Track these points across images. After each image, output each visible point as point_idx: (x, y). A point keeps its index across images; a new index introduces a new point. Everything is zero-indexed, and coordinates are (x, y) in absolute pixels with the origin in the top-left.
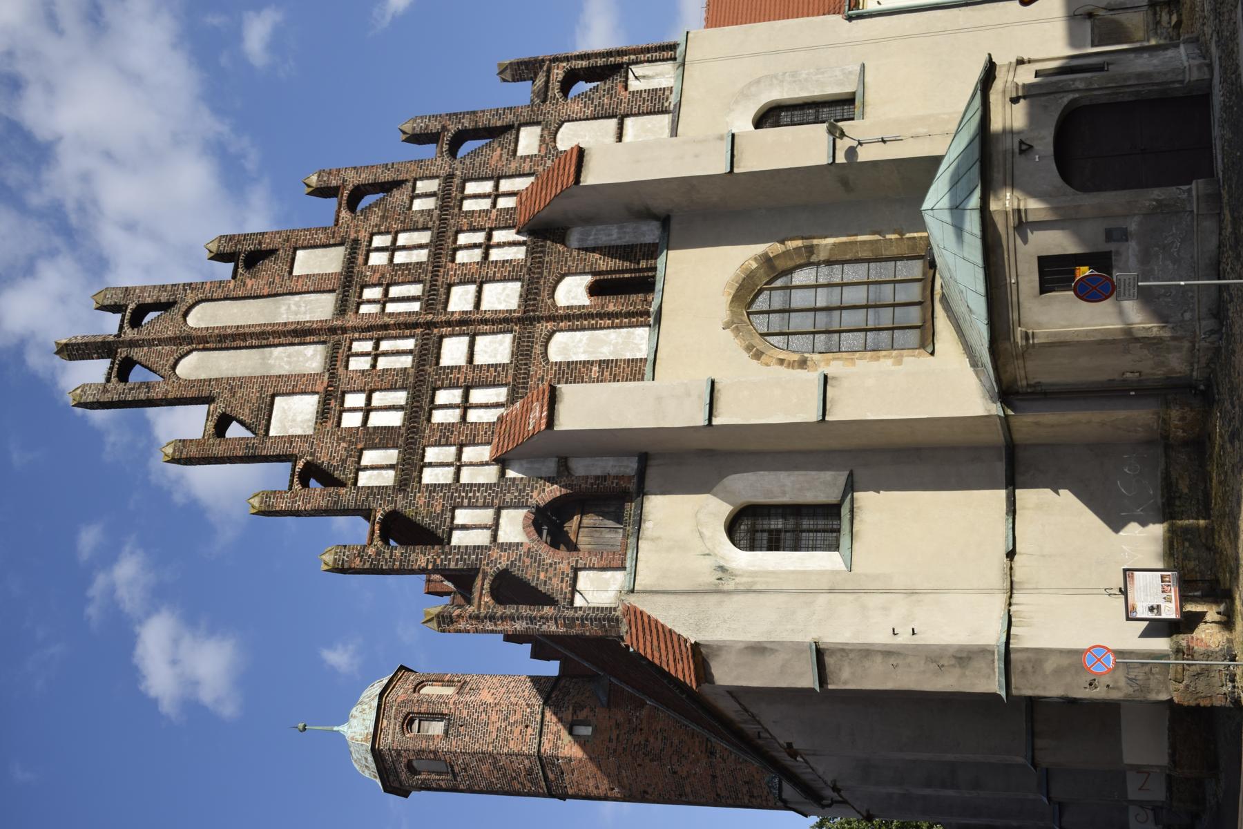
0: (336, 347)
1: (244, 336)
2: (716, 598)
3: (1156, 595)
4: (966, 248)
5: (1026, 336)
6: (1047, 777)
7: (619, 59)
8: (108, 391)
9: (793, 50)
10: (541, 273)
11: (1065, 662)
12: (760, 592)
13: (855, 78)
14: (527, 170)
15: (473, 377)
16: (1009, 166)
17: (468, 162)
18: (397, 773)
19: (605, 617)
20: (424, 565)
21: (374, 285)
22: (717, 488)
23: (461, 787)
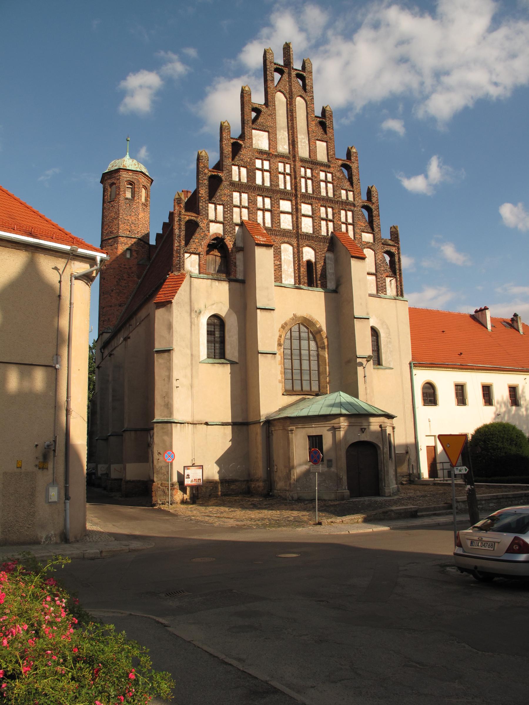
0: (288, 158)
1: (292, 120)
2: (189, 311)
3: (193, 477)
4: (326, 408)
5: (292, 430)
6: (119, 435)
7: (398, 274)
9: (399, 342)
10: (316, 242)
11: (168, 444)
12: (191, 328)
13: (388, 365)
14: (356, 236)
15: (275, 213)
16: (356, 424)
17: (360, 213)
18: (110, 178)
19: (181, 266)
20: (201, 192)
21: (312, 174)
22: (231, 311)
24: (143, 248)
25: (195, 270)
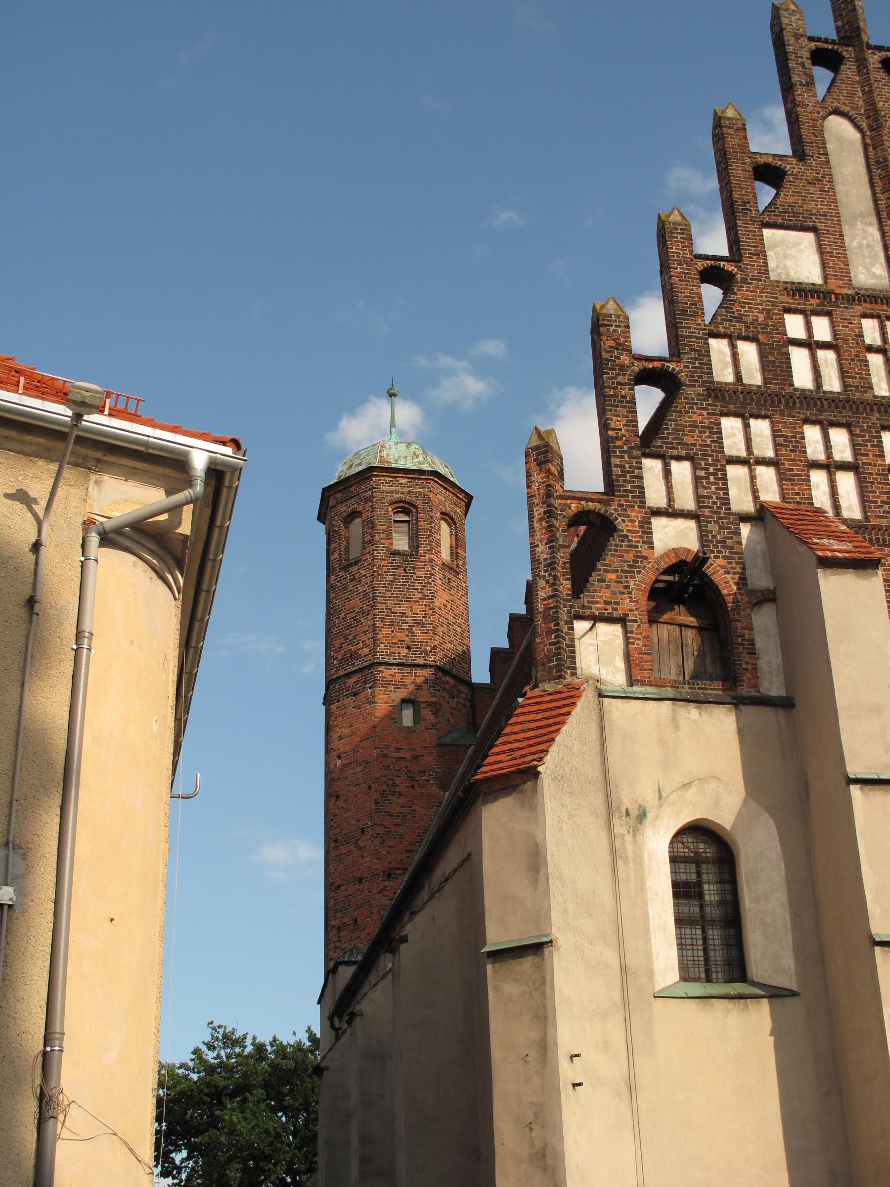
2: (601, 808)
8: (797, 39)
19: (564, 659)
20: (612, 425)
22: (752, 802)
23: (333, 577)
24: (452, 696)
25: (614, 674)
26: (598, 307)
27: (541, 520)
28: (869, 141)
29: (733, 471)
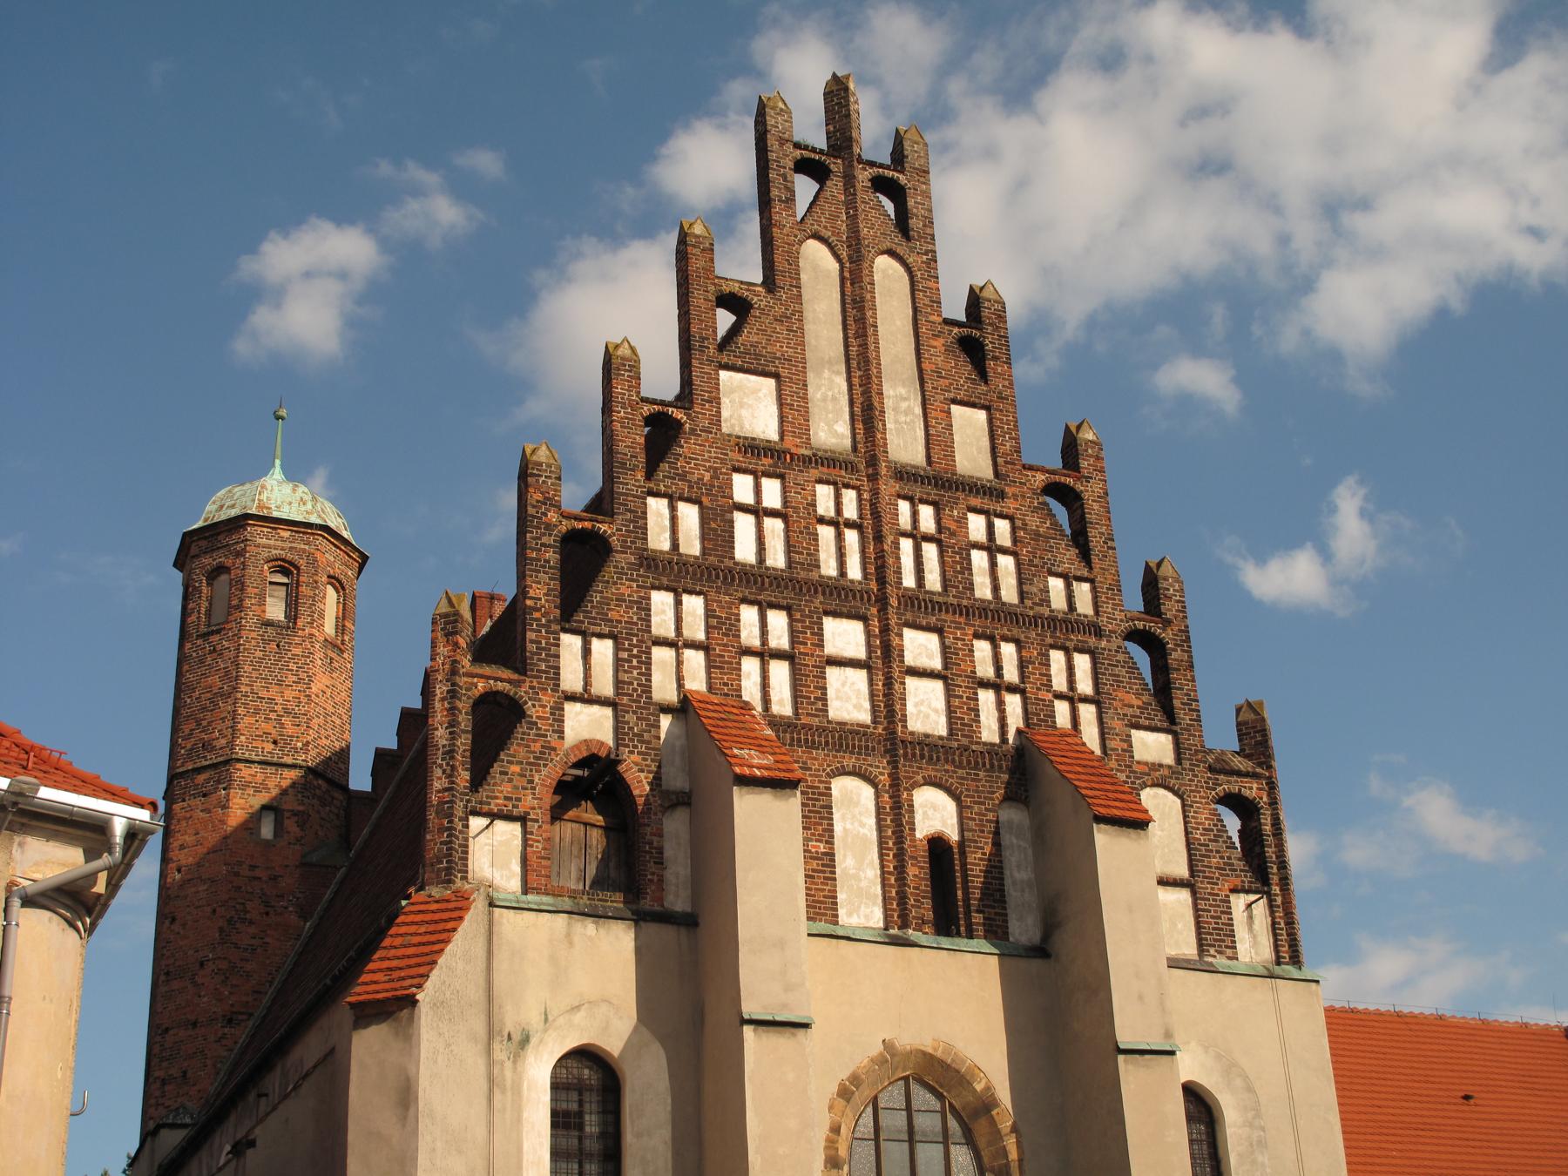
15: (808, 663)
20: (532, 593)
23: (188, 645)
26: (528, 451)
27: (443, 699)
28: (847, 275)
29: (662, 655)
